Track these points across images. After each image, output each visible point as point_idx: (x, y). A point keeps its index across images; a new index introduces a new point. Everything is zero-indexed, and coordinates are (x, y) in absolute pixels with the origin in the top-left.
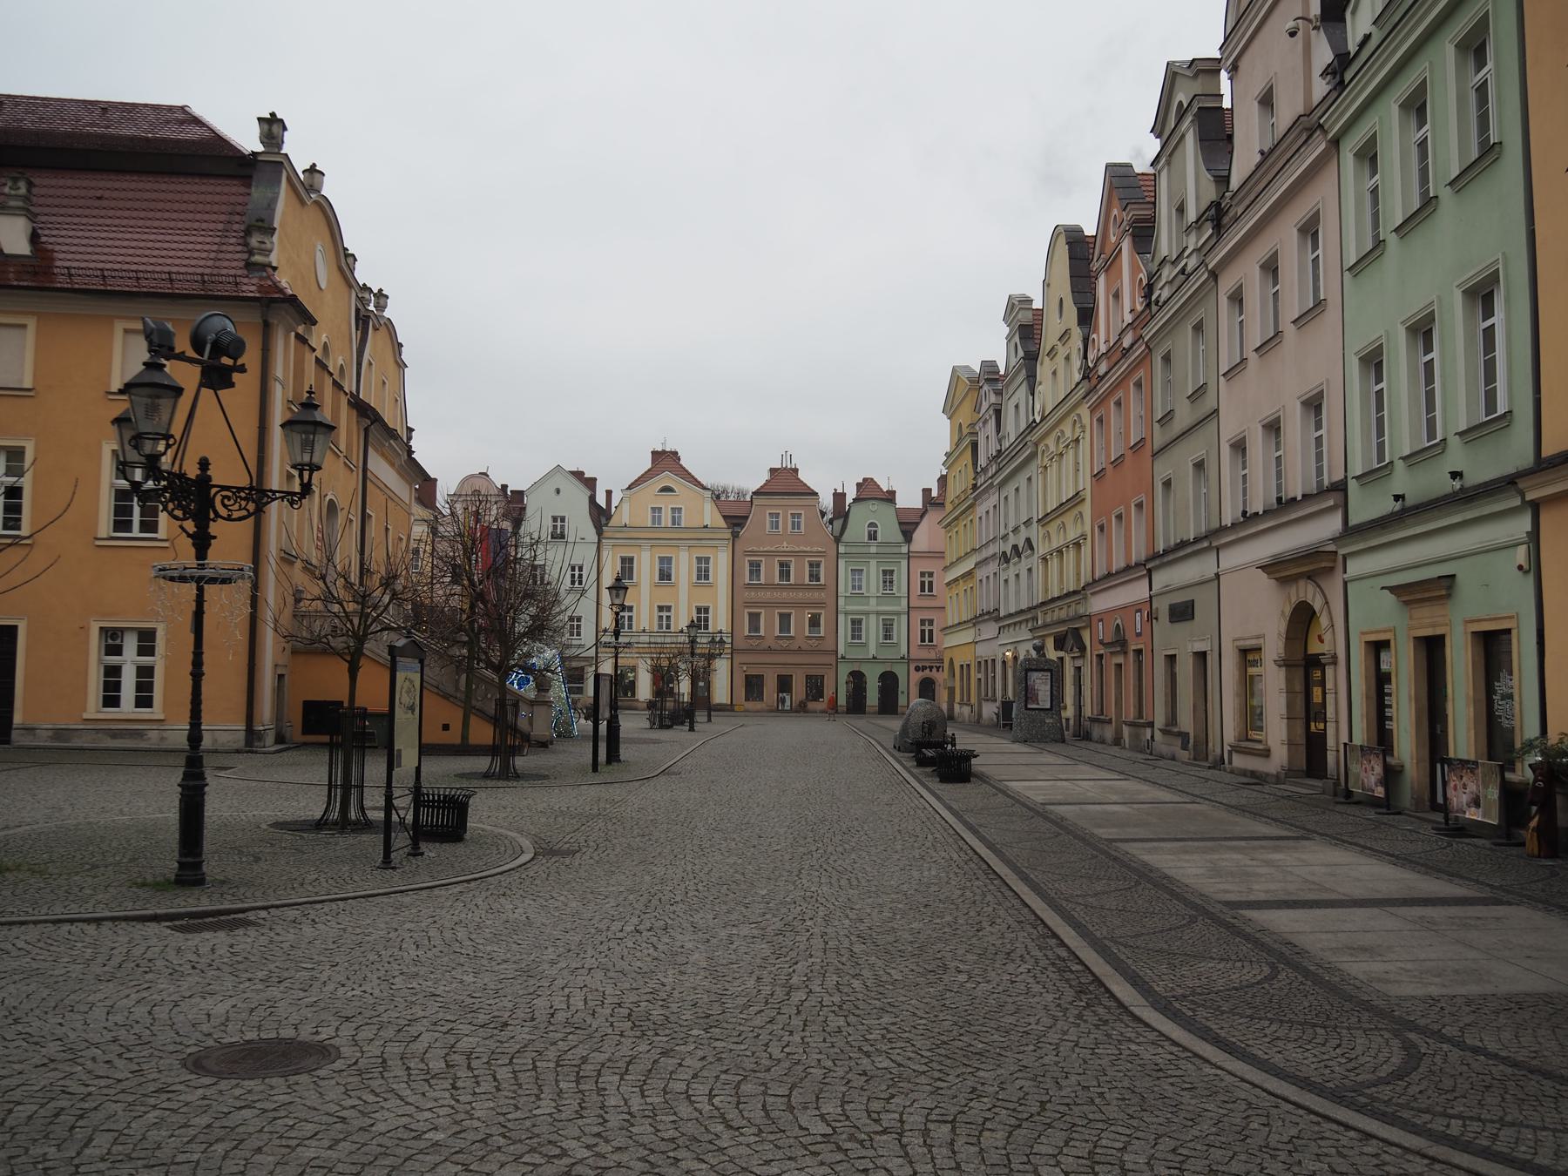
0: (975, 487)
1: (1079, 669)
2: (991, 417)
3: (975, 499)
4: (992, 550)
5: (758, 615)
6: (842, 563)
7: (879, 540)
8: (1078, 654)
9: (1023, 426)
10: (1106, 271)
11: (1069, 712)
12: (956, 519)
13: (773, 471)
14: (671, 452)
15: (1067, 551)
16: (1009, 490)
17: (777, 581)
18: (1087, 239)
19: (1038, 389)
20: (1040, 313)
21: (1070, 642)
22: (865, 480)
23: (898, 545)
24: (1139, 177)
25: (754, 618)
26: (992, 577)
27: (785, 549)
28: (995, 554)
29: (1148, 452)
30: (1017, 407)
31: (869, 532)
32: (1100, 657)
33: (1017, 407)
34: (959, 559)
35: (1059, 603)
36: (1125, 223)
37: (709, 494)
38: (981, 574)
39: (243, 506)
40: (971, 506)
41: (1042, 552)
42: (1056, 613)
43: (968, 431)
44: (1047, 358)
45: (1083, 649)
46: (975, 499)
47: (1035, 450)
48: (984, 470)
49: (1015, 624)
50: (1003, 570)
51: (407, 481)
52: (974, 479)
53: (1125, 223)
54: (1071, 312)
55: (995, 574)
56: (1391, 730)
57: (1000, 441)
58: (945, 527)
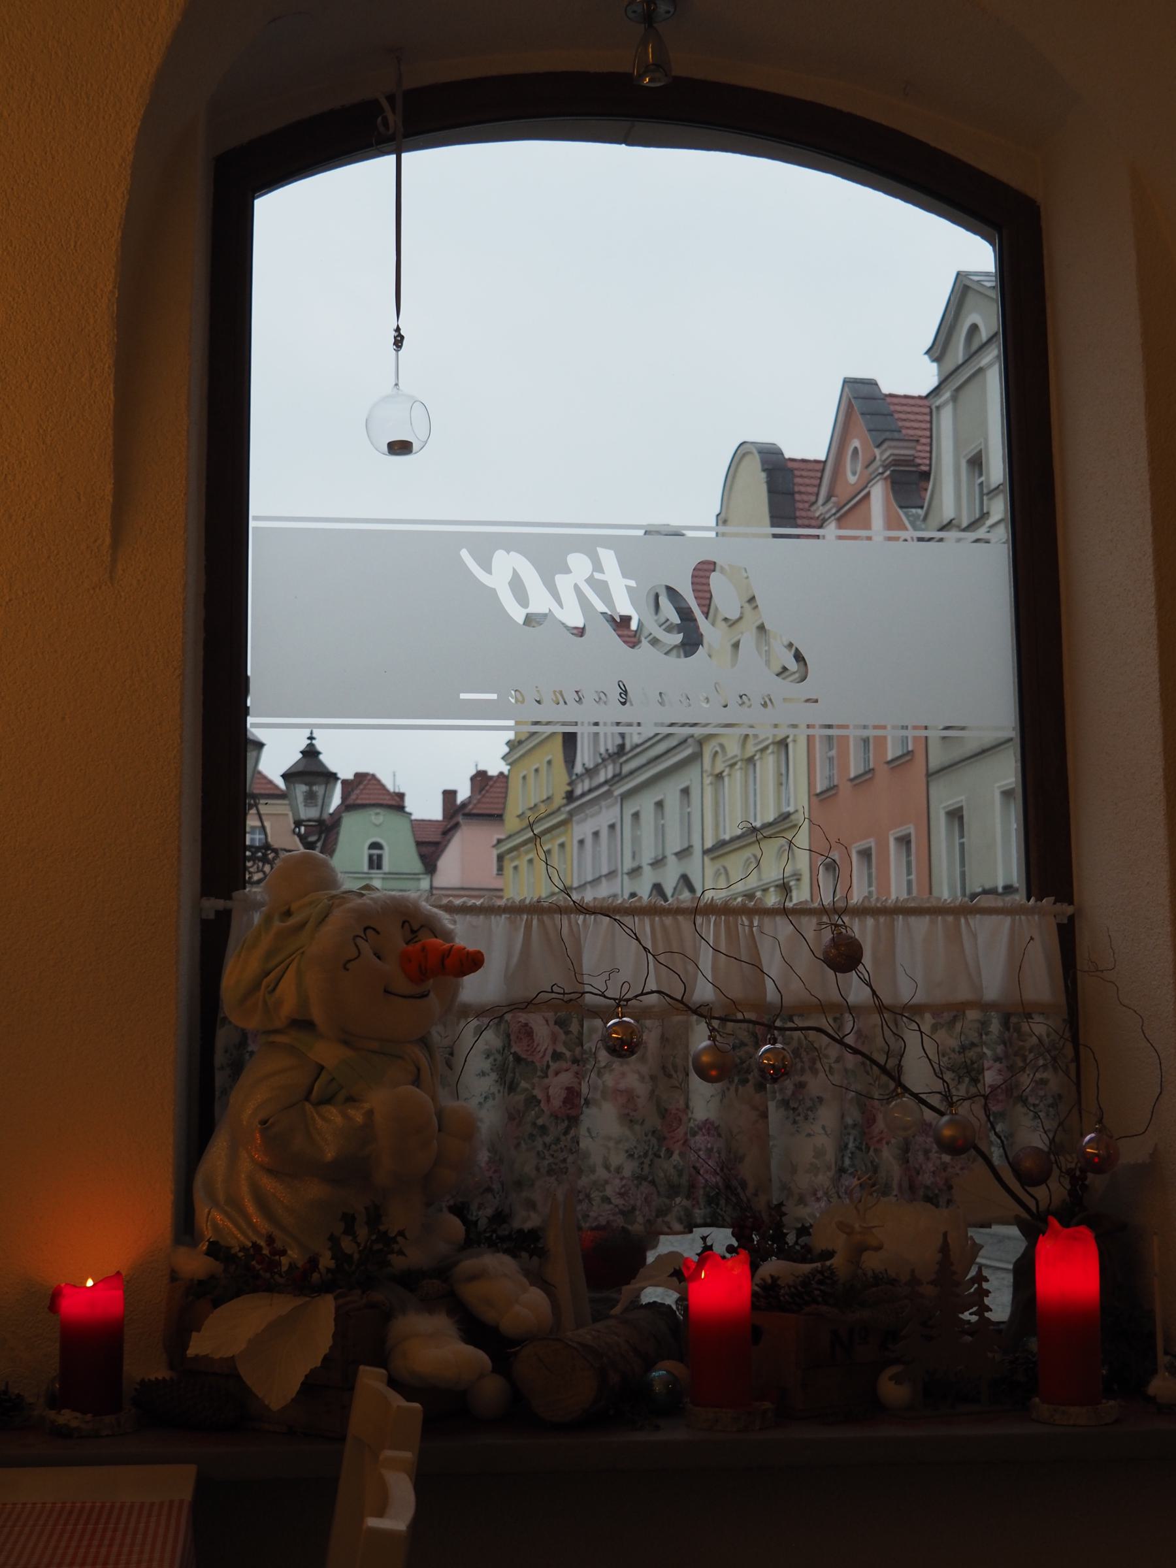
0: (570, 796)
3: (571, 814)
7: (386, 866)
18: (790, 465)
23: (414, 877)
24: (889, 400)
29: (918, 769)
31: (371, 857)
36: (877, 463)
39: (260, 868)
46: (571, 814)
47: (697, 749)
48: (590, 772)
51: (400, 811)
52: (570, 784)
53: (877, 463)
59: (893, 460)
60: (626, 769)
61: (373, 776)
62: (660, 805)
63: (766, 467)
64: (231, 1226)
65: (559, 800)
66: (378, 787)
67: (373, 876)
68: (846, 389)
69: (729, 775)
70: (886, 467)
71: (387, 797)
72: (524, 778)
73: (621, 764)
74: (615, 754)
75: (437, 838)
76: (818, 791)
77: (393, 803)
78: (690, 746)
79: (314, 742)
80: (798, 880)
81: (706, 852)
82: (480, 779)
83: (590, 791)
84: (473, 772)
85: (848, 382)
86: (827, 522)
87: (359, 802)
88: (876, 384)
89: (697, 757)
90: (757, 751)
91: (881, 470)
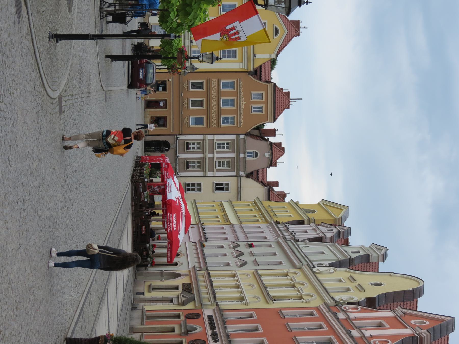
0: (278, 223)
1: (171, 301)
2: (318, 234)
3: (270, 224)
4: (241, 236)
5: (202, 106)
6: (233, 137)
7: (248, 159)
8: (180, 302)
9: (311, 258)
10: (395, 317)
11: (147, 295)
12: (260, 210)
13: (288, 94)
14: (299, 32)
15: (239, 292)
16: (275, 249)
17: (223, 98)
18: (415, 300)
19: (332, 269)
20: (376, 270)
21: (188, 296)
22: (283, 149)
24: (446, 336)
25: (200, 85)
26: (224, 236)
27: (242, 103)
28: (238, 238)
30: (323, 253)
32: (178, 316)
33: (323, 253)
34: (236, 212)
35: (209, 287)
37: (274, 57)
38: (227, 228)
40: (267, 221)
41: (238, 273)
42: (204, 284)
43: (311, 217)
44: (348, 275)
45: (183, 304)
46: (270, 224)
47: (298, 267)
49: (198, 254)
50: (229, 245)
53: (420, 331)
54: (373, 293)
55: (227, 238)
56: (138, 43)
57: (303, 241)
58: (255, 202)
59: (422, 337)
60: (289, 242)
61: (283, 154)
62: (275, 254)
63: (414, 290)
64: (144, 230)
65: (275, 219)
66: (279, 156)
67: (245, 153)
68: (450, 319)
69: (288, 279)
70: (419, 334)
71: (275, 159)
72: (284, 207)
73: (291, 241)
74: (295, 238)
75: (260, 180)
76: (282, 311)
77: (273, 161)
78: (299, 264)
79: (306, 3)
80: (245, 304)
81: (256, 271)
82: (283, 195)
83: (280, 230)
84: (286, 192)
85: (453, 319)
86: (393, 312)
87: (273, 148)
88: (452, 331)
89: (295, 267)
90: (298, 288)
91: (417, 332)
